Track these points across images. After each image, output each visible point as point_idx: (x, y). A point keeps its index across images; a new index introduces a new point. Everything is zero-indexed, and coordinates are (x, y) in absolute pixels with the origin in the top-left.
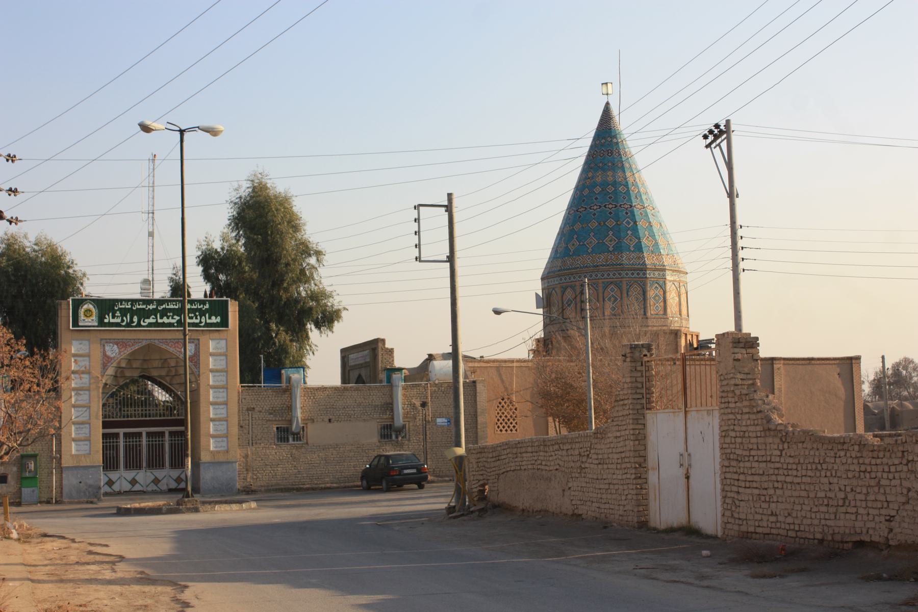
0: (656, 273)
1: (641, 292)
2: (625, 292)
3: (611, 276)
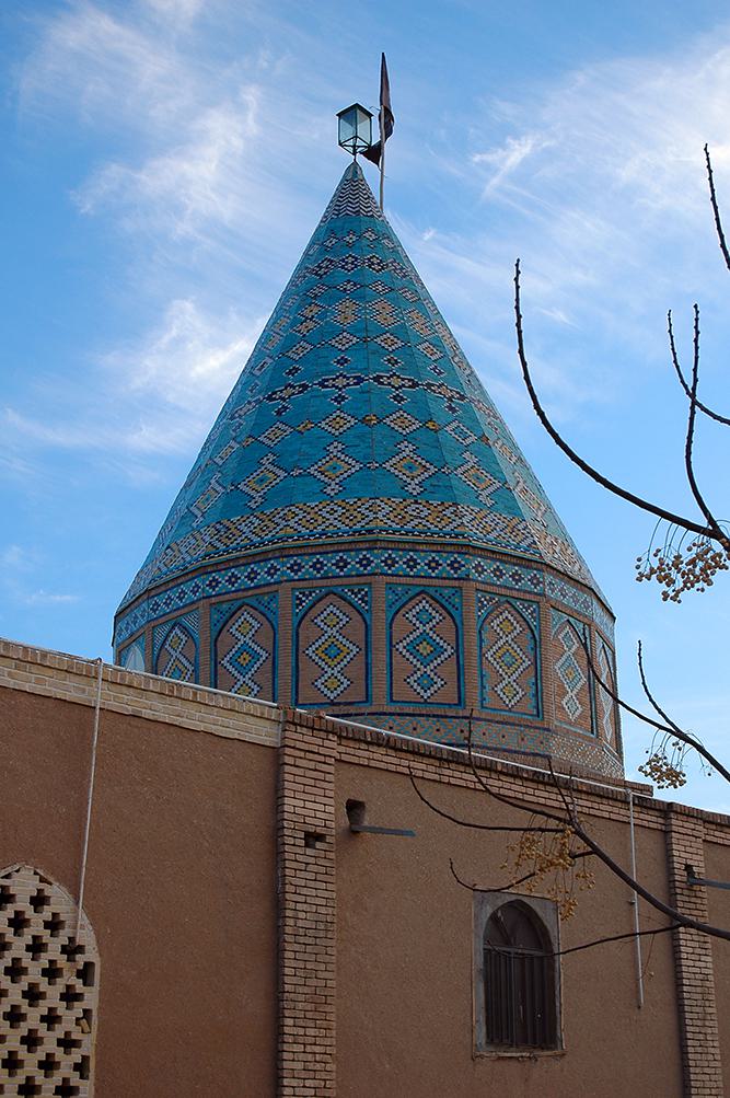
2: (473, 624)
3: (422, 568)
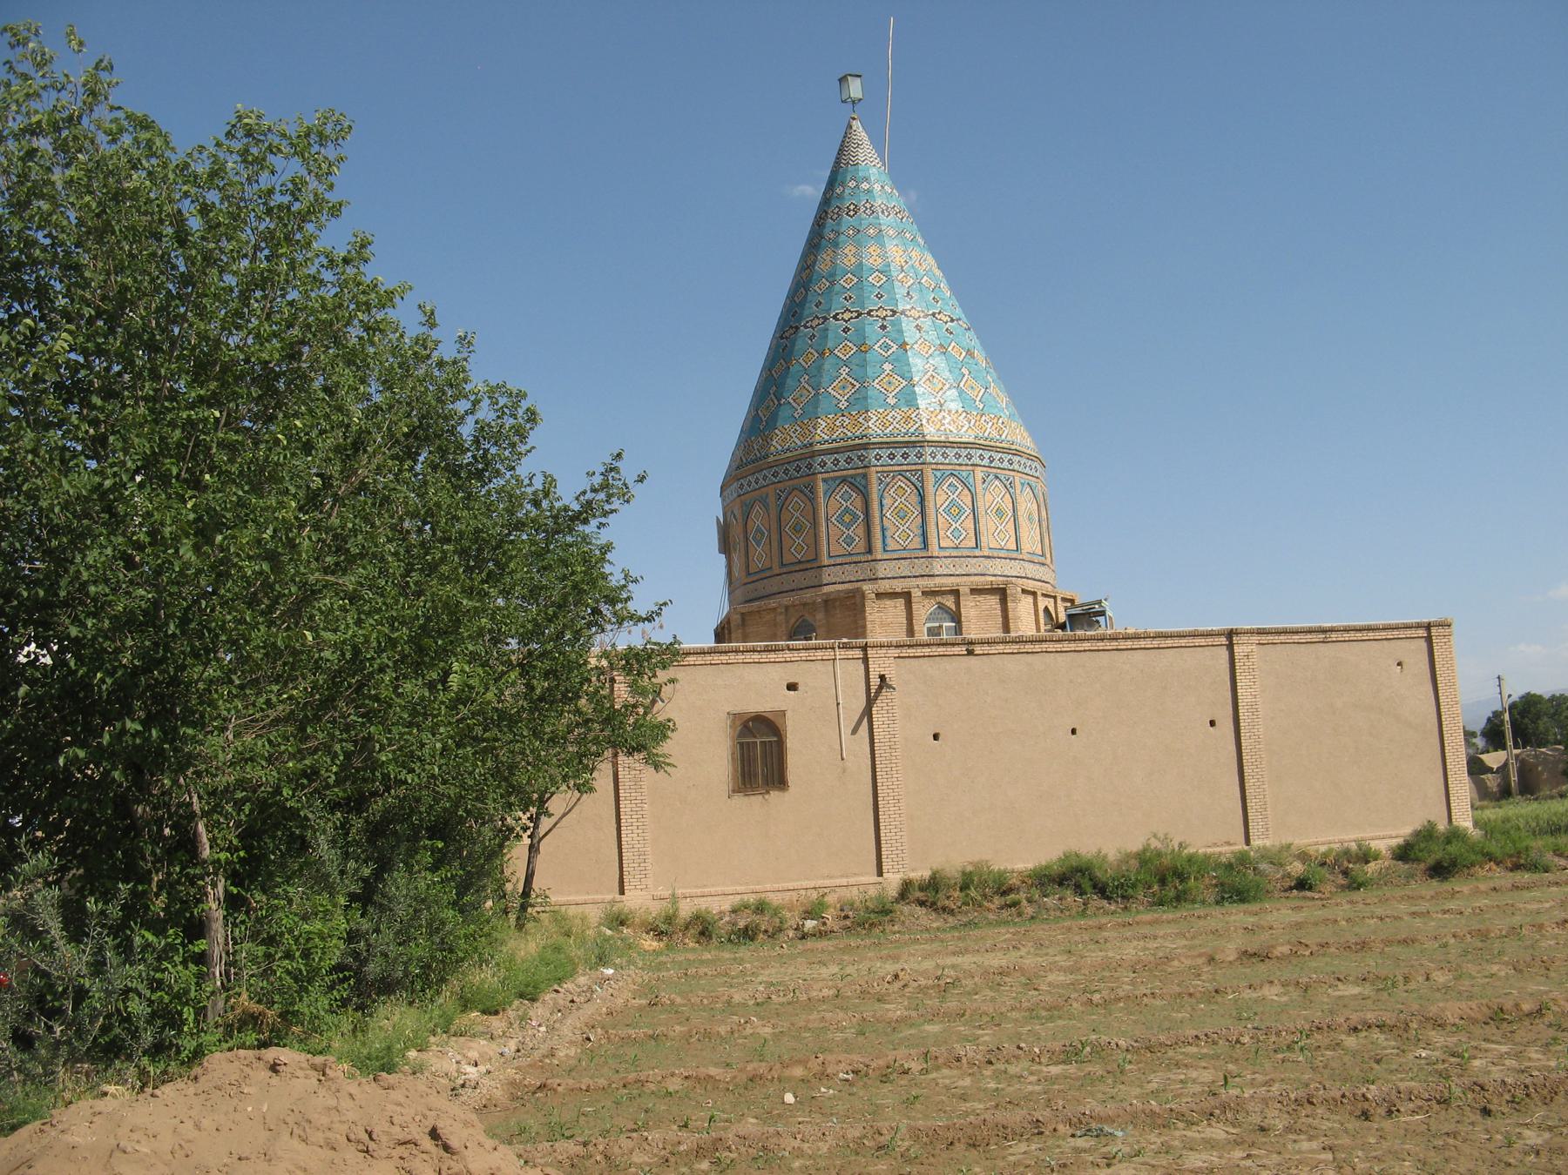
0: (951, 452)
1: (915, 499)
